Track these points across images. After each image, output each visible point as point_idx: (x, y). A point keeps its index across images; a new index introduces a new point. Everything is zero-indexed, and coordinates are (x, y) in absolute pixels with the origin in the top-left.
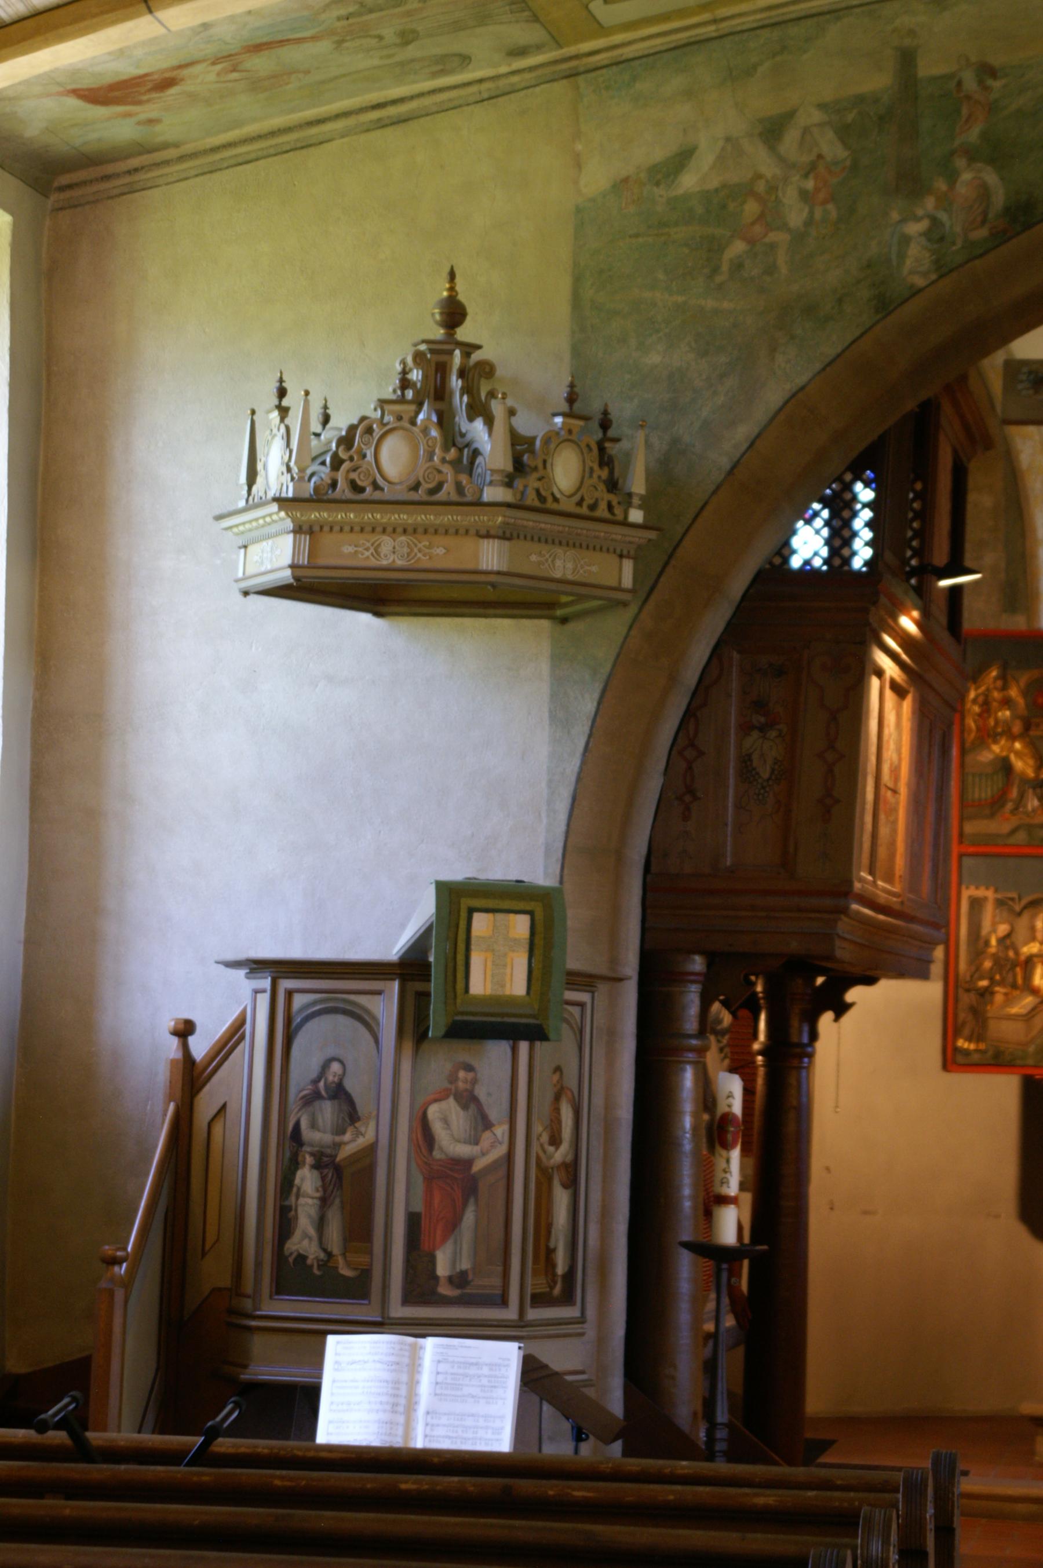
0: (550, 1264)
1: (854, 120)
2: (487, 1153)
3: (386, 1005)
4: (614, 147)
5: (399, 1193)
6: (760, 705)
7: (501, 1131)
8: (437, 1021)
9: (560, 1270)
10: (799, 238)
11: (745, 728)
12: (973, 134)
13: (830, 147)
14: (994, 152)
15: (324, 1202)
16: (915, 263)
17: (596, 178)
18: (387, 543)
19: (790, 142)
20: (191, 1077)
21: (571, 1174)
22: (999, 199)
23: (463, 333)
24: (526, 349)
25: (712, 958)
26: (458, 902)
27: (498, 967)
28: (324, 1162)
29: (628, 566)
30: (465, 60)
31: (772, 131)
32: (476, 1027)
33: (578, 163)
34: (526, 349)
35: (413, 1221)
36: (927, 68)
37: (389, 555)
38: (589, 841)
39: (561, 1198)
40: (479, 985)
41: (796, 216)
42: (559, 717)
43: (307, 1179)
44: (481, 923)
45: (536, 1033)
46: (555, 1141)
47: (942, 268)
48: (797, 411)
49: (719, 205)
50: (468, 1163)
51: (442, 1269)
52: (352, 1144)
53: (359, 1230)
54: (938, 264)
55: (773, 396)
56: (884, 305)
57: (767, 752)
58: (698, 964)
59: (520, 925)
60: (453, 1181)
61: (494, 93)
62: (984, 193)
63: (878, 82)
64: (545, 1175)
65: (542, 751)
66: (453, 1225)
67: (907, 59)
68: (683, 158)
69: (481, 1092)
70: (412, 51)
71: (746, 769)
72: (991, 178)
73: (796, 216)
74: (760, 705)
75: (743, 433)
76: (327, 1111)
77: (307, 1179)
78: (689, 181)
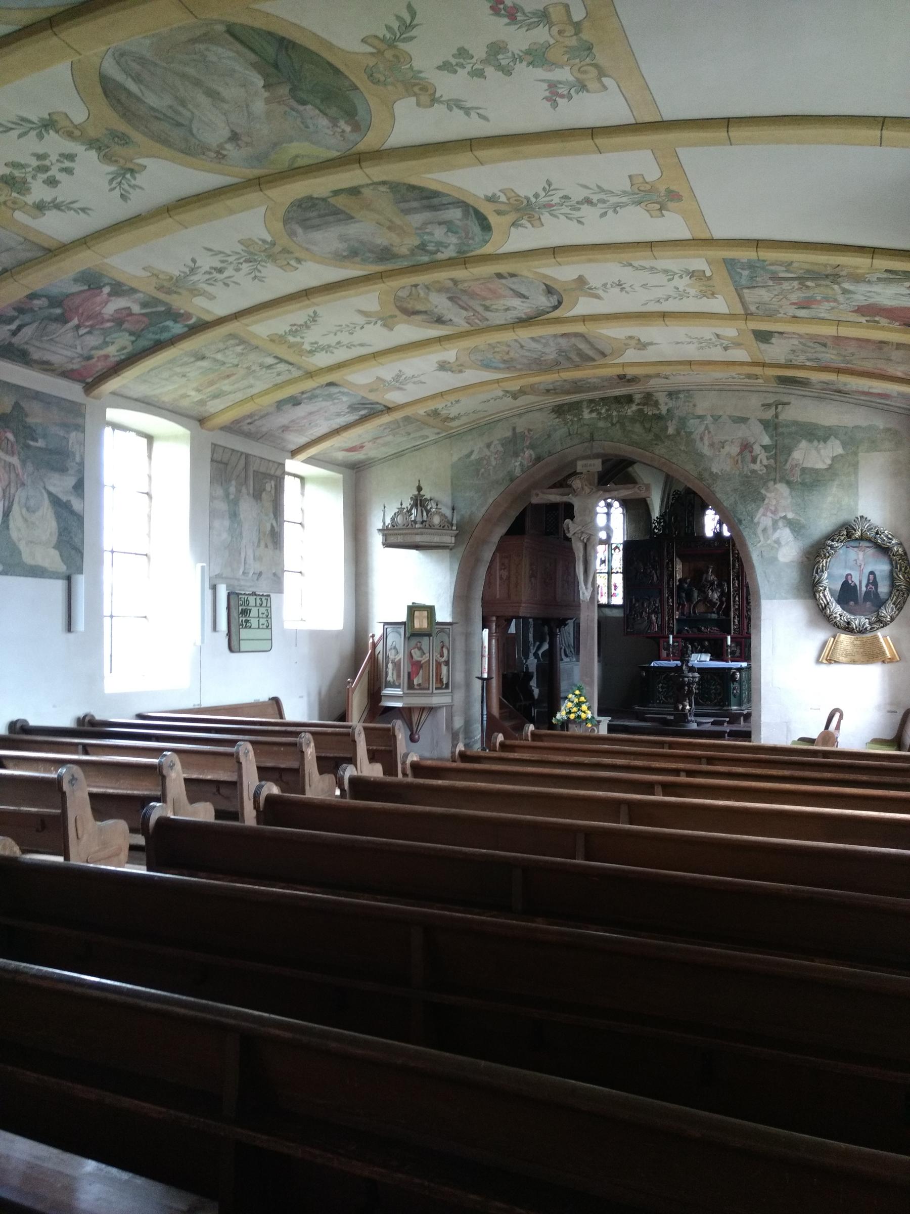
0: (441, 680)
1: (505, 443)
2: (424, 659)
4: (456, 453)
6: (503, 564)
7: (427, 655)
10: (494, 467)
11: (501, 569)
12: (528, 443)
13: (500, 448)
14: (532, 447)
16: (518, 472)
17: (455, 458)
21: (447, 663)
22: (533, 457)
23: (422, 493)
24: (439, 494)
25: (498, 617)
26: (413, 609)
29: (453, 539)
30: (427, 437)
33: (452, 455)
34: (439, 494)
35: (409, 674)
36: (518, 430)
37: (400, 539)
39: (444, 669)
40: (417, 625)
41: (494, 463)
42: (451, 569)
43: (390, 665)
44: (417, 613)
46: (442, 656)
47: (523, 471)
48: (495, 504)
49: (479, 461)
51: (415, 683)
54: (522, 470)
55: (491, 501)
56: (512, 481)
57: (505, 574)
58: (494, 618)
59: (425, 613)
62: (531, 455)
63: (509, 434)
64: (439, 664)
65: (448, 577)
66: (418, 674)
67: (514, 429)
68: (472, 452)
69: (423, 647)
70: (412, 436)
71: (501, 578)
72: (531, 452)
73: (494, 463)
74: (503, 564)
75: (485, 508)
76: (393, 651)
78: (473, 457)
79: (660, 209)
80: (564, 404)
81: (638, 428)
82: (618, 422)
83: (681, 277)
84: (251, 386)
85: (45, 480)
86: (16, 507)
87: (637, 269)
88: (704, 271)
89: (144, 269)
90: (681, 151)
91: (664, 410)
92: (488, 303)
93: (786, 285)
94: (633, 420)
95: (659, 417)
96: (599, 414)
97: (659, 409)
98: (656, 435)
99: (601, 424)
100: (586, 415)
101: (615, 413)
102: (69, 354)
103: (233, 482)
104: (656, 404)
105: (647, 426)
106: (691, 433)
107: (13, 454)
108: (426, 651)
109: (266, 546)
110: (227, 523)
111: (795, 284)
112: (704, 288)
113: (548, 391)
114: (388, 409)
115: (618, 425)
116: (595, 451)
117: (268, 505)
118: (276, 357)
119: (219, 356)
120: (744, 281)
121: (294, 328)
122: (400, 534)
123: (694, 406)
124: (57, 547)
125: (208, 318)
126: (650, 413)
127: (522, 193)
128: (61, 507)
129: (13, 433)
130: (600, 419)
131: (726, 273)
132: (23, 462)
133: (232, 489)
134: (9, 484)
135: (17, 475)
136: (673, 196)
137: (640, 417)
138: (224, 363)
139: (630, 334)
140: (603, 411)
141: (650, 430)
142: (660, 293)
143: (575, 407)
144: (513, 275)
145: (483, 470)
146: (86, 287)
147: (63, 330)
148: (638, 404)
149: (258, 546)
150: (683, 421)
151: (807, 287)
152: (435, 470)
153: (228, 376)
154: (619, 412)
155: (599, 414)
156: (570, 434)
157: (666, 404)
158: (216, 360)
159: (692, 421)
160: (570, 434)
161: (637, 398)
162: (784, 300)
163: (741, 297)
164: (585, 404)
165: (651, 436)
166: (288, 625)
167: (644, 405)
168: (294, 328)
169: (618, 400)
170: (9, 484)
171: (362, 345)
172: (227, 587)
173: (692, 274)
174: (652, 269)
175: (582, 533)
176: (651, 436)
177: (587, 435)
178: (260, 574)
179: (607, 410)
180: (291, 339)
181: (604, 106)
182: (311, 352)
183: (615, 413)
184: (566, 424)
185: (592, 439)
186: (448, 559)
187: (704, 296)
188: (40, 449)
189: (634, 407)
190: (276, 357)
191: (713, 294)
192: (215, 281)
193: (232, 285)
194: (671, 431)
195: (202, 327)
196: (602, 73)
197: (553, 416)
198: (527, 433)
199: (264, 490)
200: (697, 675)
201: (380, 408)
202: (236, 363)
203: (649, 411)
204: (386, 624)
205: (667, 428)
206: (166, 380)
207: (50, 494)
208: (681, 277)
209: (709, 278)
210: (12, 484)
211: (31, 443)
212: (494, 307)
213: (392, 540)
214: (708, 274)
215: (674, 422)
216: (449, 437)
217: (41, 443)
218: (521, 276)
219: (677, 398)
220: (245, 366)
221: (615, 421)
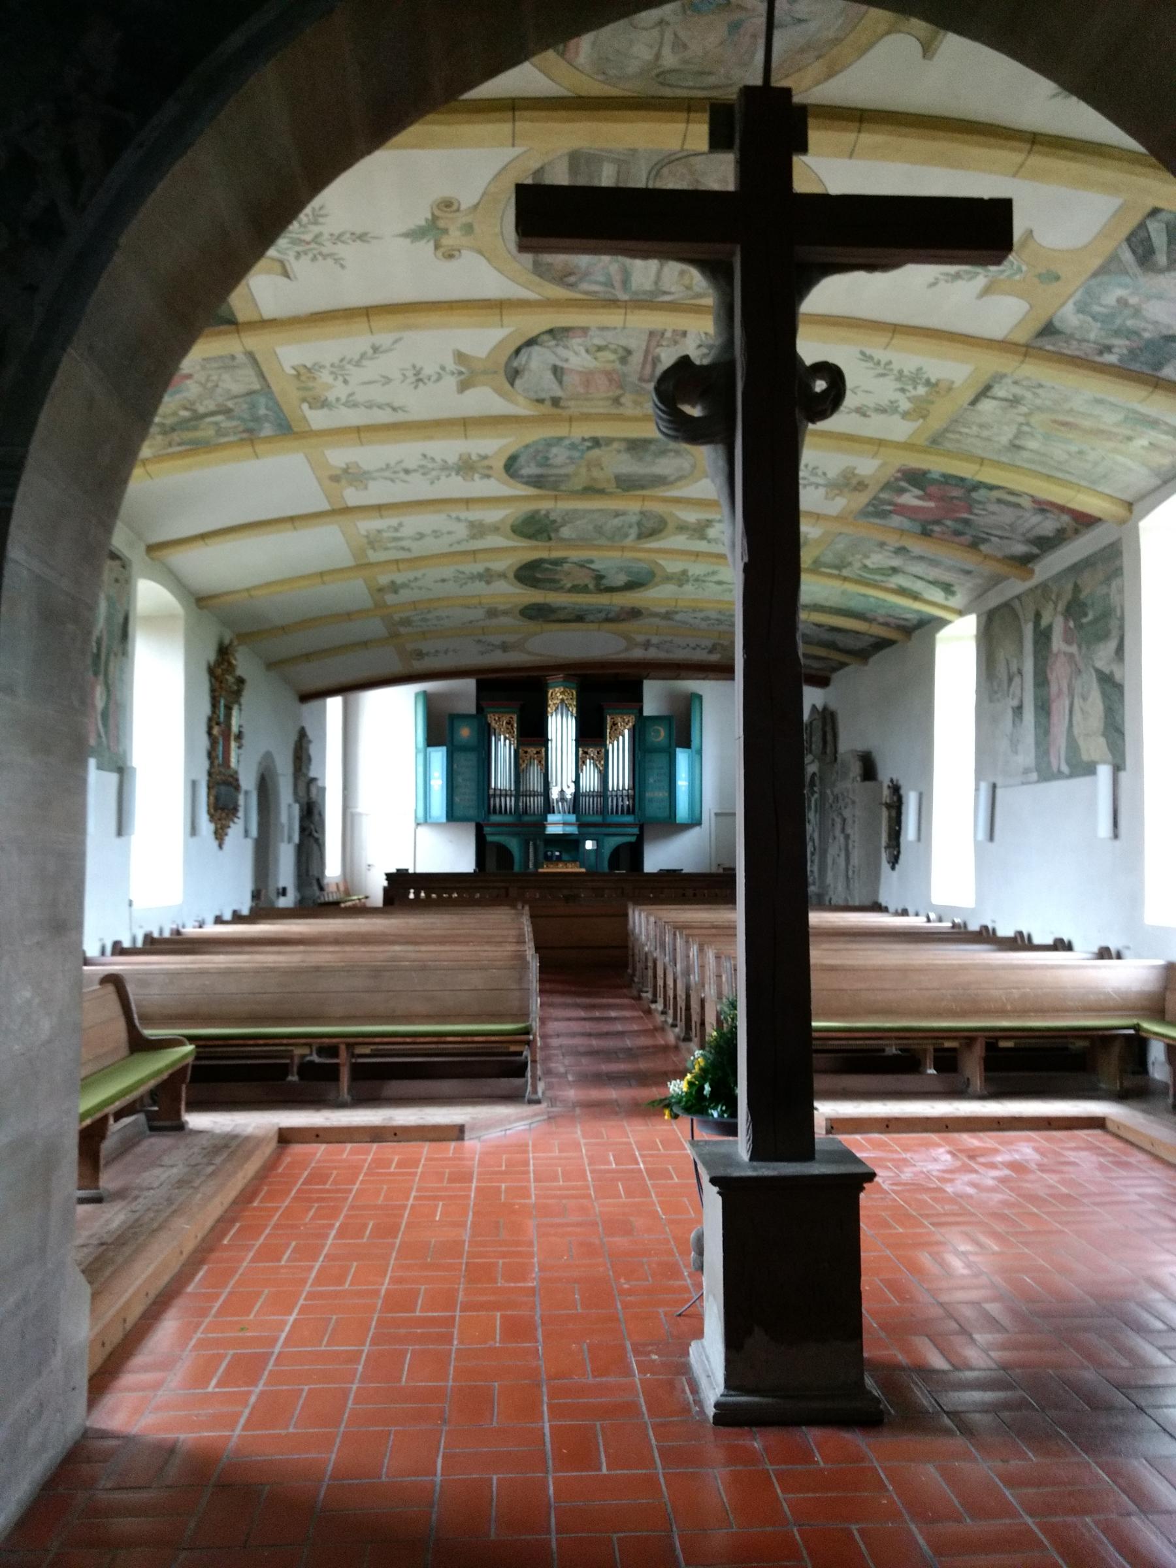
79: (348, 468)
83: (338, 400)
87: (388, 405)
88: (310, 408)
89: (1058, 278)
90: (278, 350)
92: (618, 365)
93: (212, 406)
111: (201, 410)
112: (311, 384)
116: (1081, 742)
120: (262, 400)
124: (1104, 735)
127: (460, 478)
131: (285, 407)
136: (335, 479)
142: (372, 370)
144: (541, 401)
151: (186, 409)
162: (203, 380)
163: (262, 376)
173: (324, 404)
174: (370, 405)
181: (368, 525)
187: (309, 370)
191: (298, 375)
196: (367, 537)
200: (1103, 1086)
208: (338, 400)
209: (304, 400)
212: (612, 357)
214: (305, 406)
218: (531, 400)
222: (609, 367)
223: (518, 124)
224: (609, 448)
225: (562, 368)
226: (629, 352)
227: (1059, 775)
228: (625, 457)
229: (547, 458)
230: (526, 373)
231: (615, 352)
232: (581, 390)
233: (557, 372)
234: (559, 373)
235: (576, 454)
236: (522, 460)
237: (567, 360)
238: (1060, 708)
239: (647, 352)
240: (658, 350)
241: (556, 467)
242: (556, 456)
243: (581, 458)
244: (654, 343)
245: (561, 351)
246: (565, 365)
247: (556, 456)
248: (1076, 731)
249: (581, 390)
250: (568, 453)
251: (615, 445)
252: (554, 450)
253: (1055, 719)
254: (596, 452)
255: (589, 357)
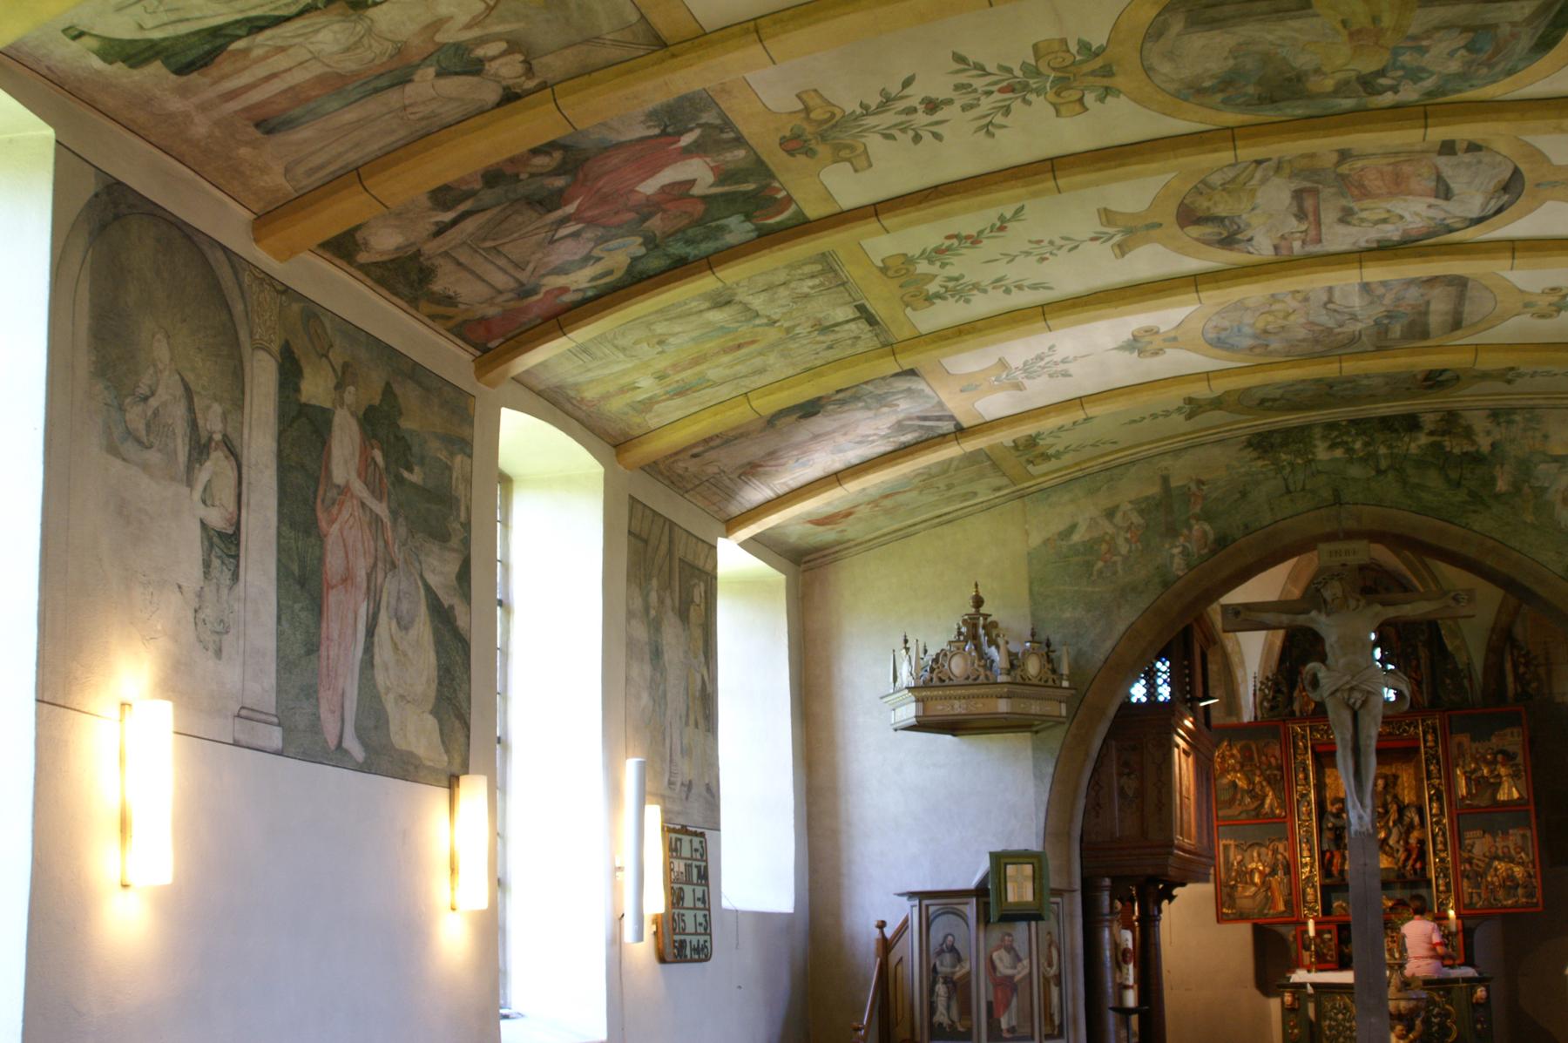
1: (1145, 507)
2: (1020, 972)
3: (970, 909)
4: (1043, 524)
5: (982, 993)
7: (1026, 962)
8: (994, 914)
9: (1057, 1022)
10: (1126, 558)
11: (1120, 775)
12: (1197, 509)
13: (1136, 519)
14: (1207, 516)
15: (949, 998)
16: (1178, 566)
17: (1036, 539)
18: (957, 703)
19: (1118, 518)
20: (886, 946)
21: (1058, 979)
22: (1211, 536)
23: (983, 610)
24: (1011, 614)
25: (1114, 879)
26: (1000, 861)
27: (1019, 889)
28: (948, 980)
29: (1063, 706)
30: (975, 494)
31: (1110, 514)
32: (1012, 916)
35: (990, 1005)
36: (1175, 483)
37: (958, 708)
38: (1054, 830)
39: (1055, 991)
41: (1124, 550)
42: (1038, 776)
43: (941, 989)
45: (1038, 917)
46: (1050, 965)
47: (1190, 567)
49: (1090, 547)
50: (1011, 977)
51: (1004, 1026)
52: (959, 972)
53: (966, 1009)
54: (1188, 565)
55: (1121, 627)
56: (1166, 585)
58: (1107, 882)
59: (1028, 869)
60: (1006, 986)
61: (989, 507)
62: (1205, 533)
63: (1154, 490)
64: (1047, 980)
65: (1031, 791)
66: (1007, 1006)
67: (1165, 480)
68: (1073, 528)
69: (1015, 945)
72: (1207, 527)
73: (1124, 550)
75: (1109, 645)
76: (948, 958)
77: (941, 989)
78: (1076, 538)
80: (1271, 432)
81: (1433, 479)
82: (1391, 467)
84: (761, 371)
85: (422, 558)
86: (383, 617)
91: (1484, 444)
92: (1355, 206)
94: (1421, 464)
95: (1476, 459)
96: (1349, 450)
97: (1474, 443)
98: (1471, 493)
99: (1355, 471)
100: (1322, 453)
101: (1383, 450)
102: (500, 280)
103: (654, 582)
104: (1468, 433)
105: (1454, 475)
106: (1544, 490)
107: (380, 500)
108: (1023, 953)
109: (696, 726)
110: (647, 669)
113: (1262, 401)
114: (961, 432)
115: (1391, 476)
117: (698, 633)
118: (861, 309)
119: (757, 302)
121: (948, 243)
122: (959, 698)
123: (1546, 437)
124: (435, 712)
125: (813, 211)
126: (1457, 451)
128: (443, 617)
129: (382, 450)
130: (1351, 461)
132: (394, 514)
133: (653, 597)
134: (375, 565)
135: (386, 543)
137: (1437, 457)
138: (757, 315)
139: (1554, 285)
140: (1358, 445)
141: (1459, 485)
143: (1296, 437)
144: (1473, 147)
145: (1100, 564)
146: (657, 131)
147: (539, 224)
148: (1431, 433)
149: (687, 724)
150: (1525, 468)
152: (997, 558)
153: (739, 347)
154: (1390, 447)
155: (1349, 450)
156: (1288, 491)
157: (1488, 433)
158: (746, 308)
159: (1542, 467)
160: (1288, 491)
161: (1429, 421)
164: (1318, 432)
165: (1462, 496)
166: (725, 904)
167: (1444, 433)
168: (948, 243)
169: (1386, 423)
170: (375, 565)
171: (1035, 287)
172: (665, 812)
175: (1352, 689)
176: (1462, 496)
177: (1326, 494)
178: (689, 786)
179: (1366, 444)
180: (923, 267)
182: (929, 299)
183: (1383, 450)
184: (1279, 469)
185: (1337, 501)
186: (1029, 753)
188: (413, 485)
189: (1423, 440)
190: (861, 309)
192: (903, 131)
193: (927, 137)
194: (1501, 485)
195: (803, 227)
197: (1250, 454)
198: (1193, 487)
199: (692, 601)
201: (947, 426)
202: (775, 317)
203: (1455, 446)
204: (921, 895)
205: (1493, 480)
206: (624, 350)
207: (428, 588)
210: (380, 565)
211: (406, 474)
212: (1364, 215)
213: (942, 709)
215: (1507, 467)
216: (1021, 496)
217: (415, 477)
218: (1489, 149)
219: (1510, 422)
220: (786, 325)
221: (1384, 464)
222: (1367, 203)
223: (1429, 130)
224: (1339, 76)
225: (1437, 197)
226: (1342, 221)
227: (337, 756)
228: (1303, 61)
229: (1470, 48)
230: (1491, 187)
231: (1362, 220)
232: (1406, 169)
233: (1444, 191)
234: (1442, 188)
235: (1406, 58)
236: (1525, 42)
237: (1430, 206)
238: (345, 614)
239: (1318, 224)
240: (1303, 227)
241: (1447, 26)
242: (1451, 54)
243: (1396, 52)
244: (1312, 233)
245: (1440, 215)
246: (1432, 201)
247: (1451, 54)
248: (380, 678)
249: (1406, 169)
250: (1426, 60)
251: (1329, 84)
252: (1454, 66)
253: (333, 626)
254: (1368, 65)
255: (1399, 211)
